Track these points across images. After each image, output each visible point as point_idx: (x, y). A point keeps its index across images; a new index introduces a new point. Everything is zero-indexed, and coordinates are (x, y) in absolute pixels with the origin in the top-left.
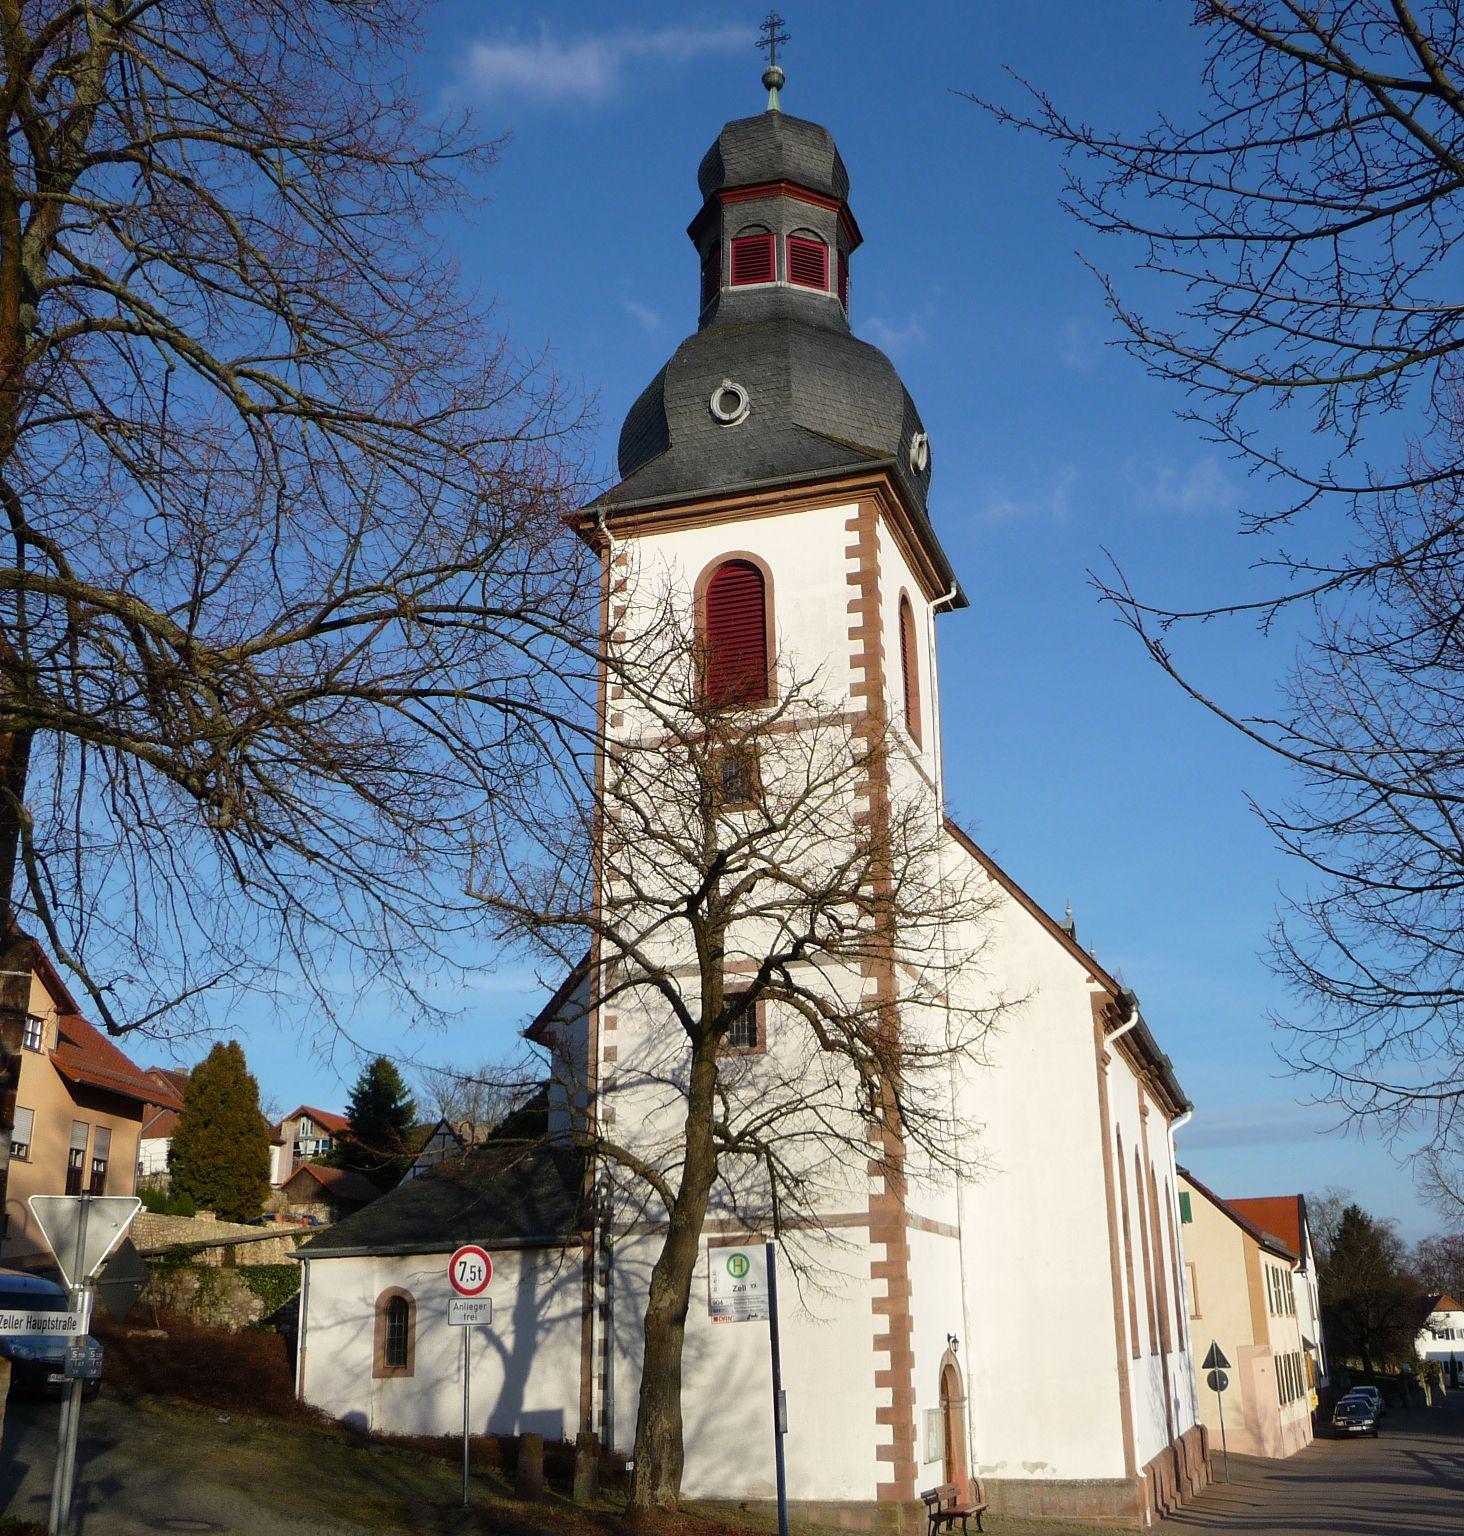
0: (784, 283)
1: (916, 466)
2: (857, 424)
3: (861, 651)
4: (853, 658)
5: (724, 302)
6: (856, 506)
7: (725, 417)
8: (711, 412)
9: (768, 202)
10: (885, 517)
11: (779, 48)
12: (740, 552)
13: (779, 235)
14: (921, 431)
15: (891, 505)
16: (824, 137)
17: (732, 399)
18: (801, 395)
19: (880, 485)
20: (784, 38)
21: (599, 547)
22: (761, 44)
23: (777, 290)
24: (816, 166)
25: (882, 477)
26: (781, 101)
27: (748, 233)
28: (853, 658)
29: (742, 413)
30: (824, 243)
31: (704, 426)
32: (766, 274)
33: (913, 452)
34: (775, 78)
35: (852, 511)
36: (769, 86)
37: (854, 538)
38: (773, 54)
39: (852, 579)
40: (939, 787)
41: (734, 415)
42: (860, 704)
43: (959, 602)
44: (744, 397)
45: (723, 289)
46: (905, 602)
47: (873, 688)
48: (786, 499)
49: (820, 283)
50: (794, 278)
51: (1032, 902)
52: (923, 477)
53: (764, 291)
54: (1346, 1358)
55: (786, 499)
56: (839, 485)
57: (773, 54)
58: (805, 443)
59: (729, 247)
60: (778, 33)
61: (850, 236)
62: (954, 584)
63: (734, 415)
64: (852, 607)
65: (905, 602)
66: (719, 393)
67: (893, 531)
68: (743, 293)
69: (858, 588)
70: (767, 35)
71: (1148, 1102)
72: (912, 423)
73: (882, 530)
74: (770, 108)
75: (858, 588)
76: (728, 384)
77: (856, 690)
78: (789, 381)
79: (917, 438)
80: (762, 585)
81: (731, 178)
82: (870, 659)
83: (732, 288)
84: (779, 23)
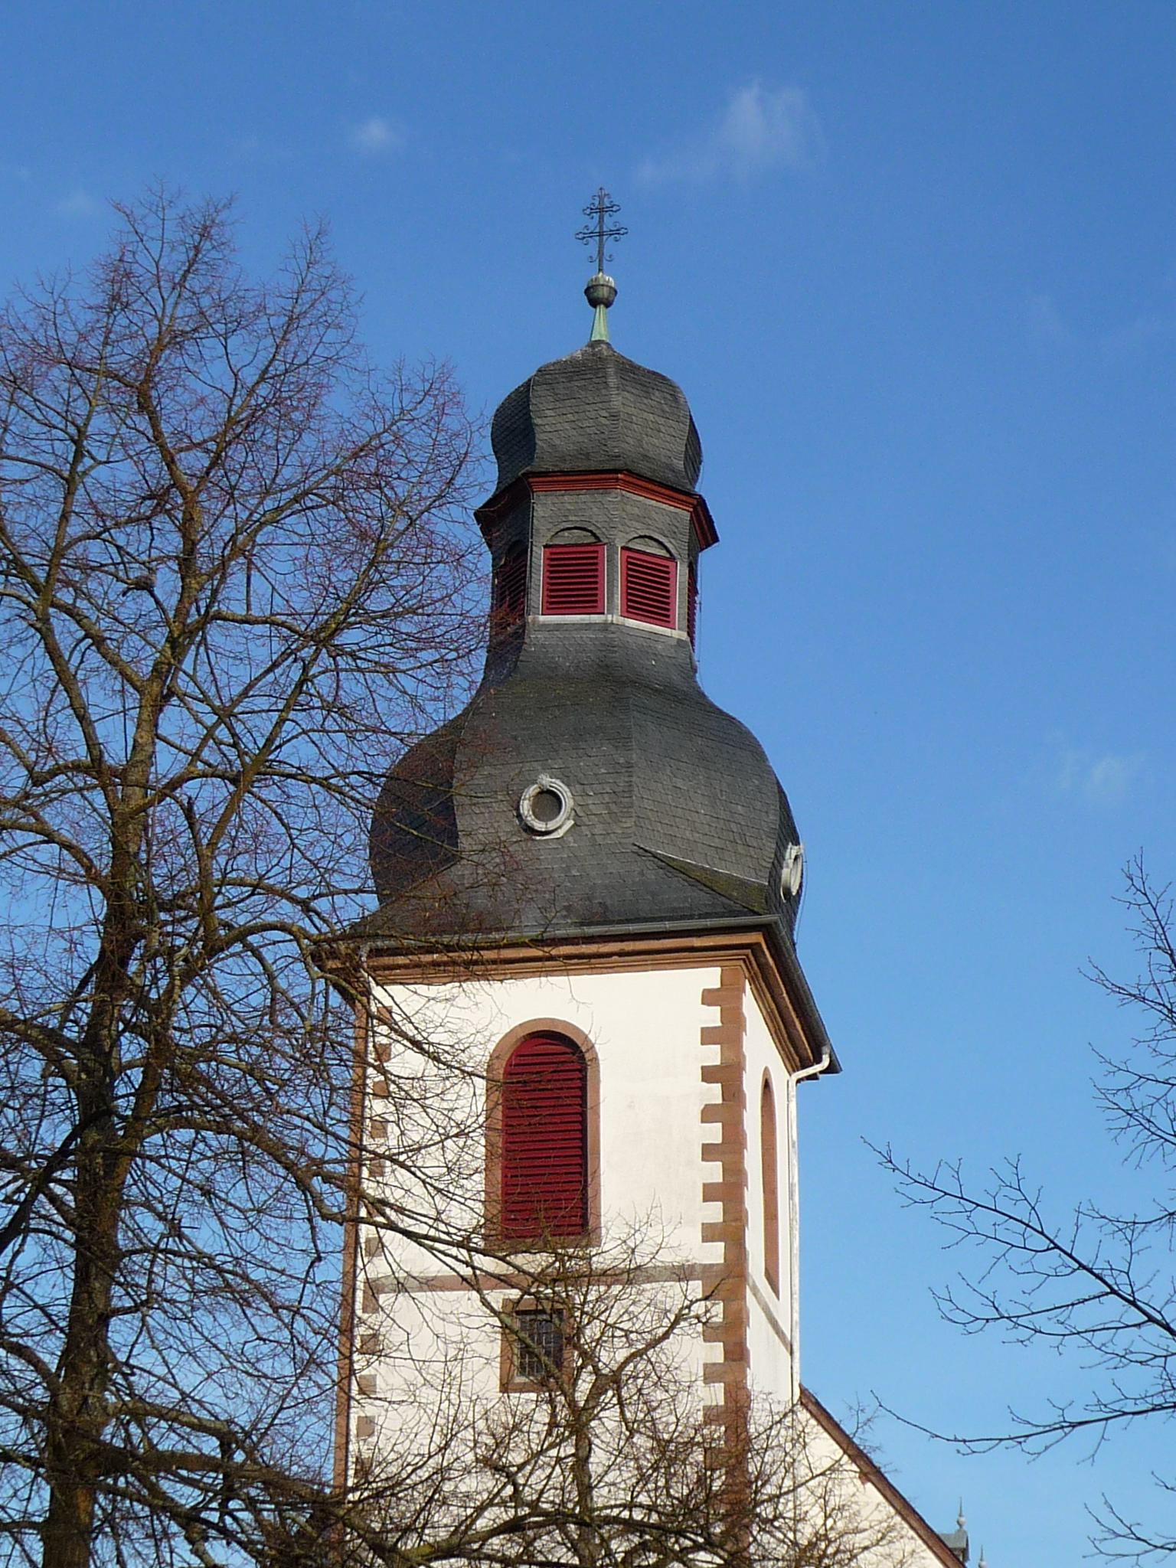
0: (616, 618)
1: (787, 891)
2: (717, 842)
3: (718, 1178)
4: (707, 1187)
5: (533, 637)
6: (719, 970)
7: (539, 826)
8: (519, 816)
9: (599, 497)
10: (752, 981)
11: (609, 243)
12: (553, 1020)
13: (612, 546)
14: (797, 842)
15: (763, 967)
16: (676, 399)
17: (549, 801)
18: (646, 804)
19: (753, 947)
20: (617, 232)
21: (354, 994)
22: (584, 236)
23: (605, 627)
24: (667, 449)
25: (756, 937)
26: (610, 325)
27: (567, 538)
28: (707, 1187)
29: (562, 824)
30: (672, 558)
31: (506, 828)
32: (590, 602)
33: (785, 872)
34: (603, 293)
35: (710, 977)
36: (594, 302)
37: (713, 1016)
38: (601, 253)
39: (709, 1075)
40: (796, 1347)
41: (551, 825)
42: (715, 1253)
43: (832, 1069)
44: (568, 802)
45: (530, 618)
46: (767, 1085)
47: (731, 1232)
48: (621, 954)
49: (662, 615)
50: (632, 609)
51: (921, 1520)
52: (792, 901)
53: (588, 626)
54: (112, 1112)
55: (621, 954)
56: (697, 942)
57: (601, 253)
58: (651, 876)
59: (539, 558)
60: (609, 223)
61: (704, 532)
62: (826, 1049)
63: (551, 825)
64: (708, 1114)
65: (767, 1085)
66: (532, 790)
67: (759, 996)
68: (558, 627)
69: (717, 1088)
70: (593, 224)
71: (411, 987)
72: (788, 833)
73: (750, 1007)
74: (596, 337)
75: (717, 1088)
76: (547, 781)
77: (710, 1233)
78: (630, 784)
79: (792, 851)
80: (583, 1070)
81: (543, 461)
82: (728, 1192)
83: (542, 618)
84: (611, 209)
